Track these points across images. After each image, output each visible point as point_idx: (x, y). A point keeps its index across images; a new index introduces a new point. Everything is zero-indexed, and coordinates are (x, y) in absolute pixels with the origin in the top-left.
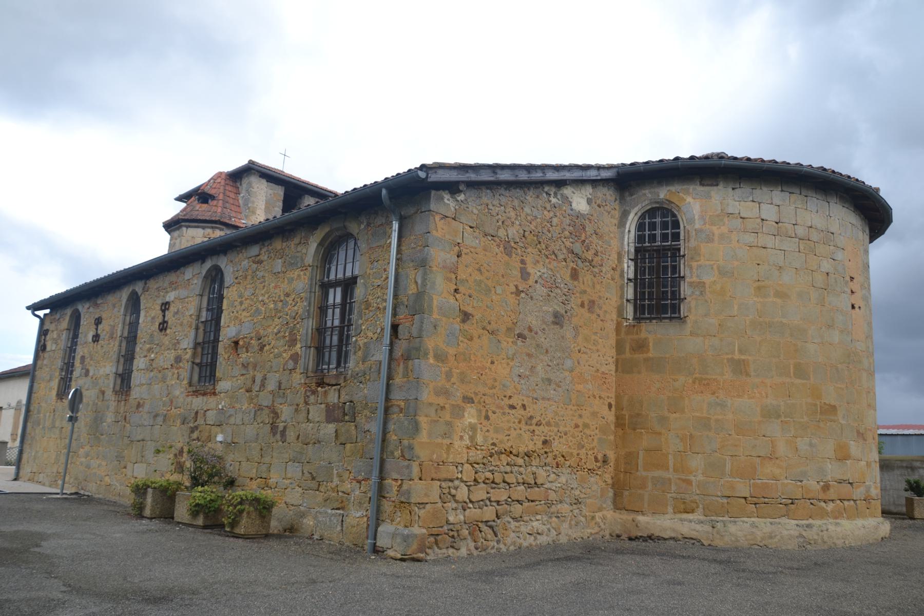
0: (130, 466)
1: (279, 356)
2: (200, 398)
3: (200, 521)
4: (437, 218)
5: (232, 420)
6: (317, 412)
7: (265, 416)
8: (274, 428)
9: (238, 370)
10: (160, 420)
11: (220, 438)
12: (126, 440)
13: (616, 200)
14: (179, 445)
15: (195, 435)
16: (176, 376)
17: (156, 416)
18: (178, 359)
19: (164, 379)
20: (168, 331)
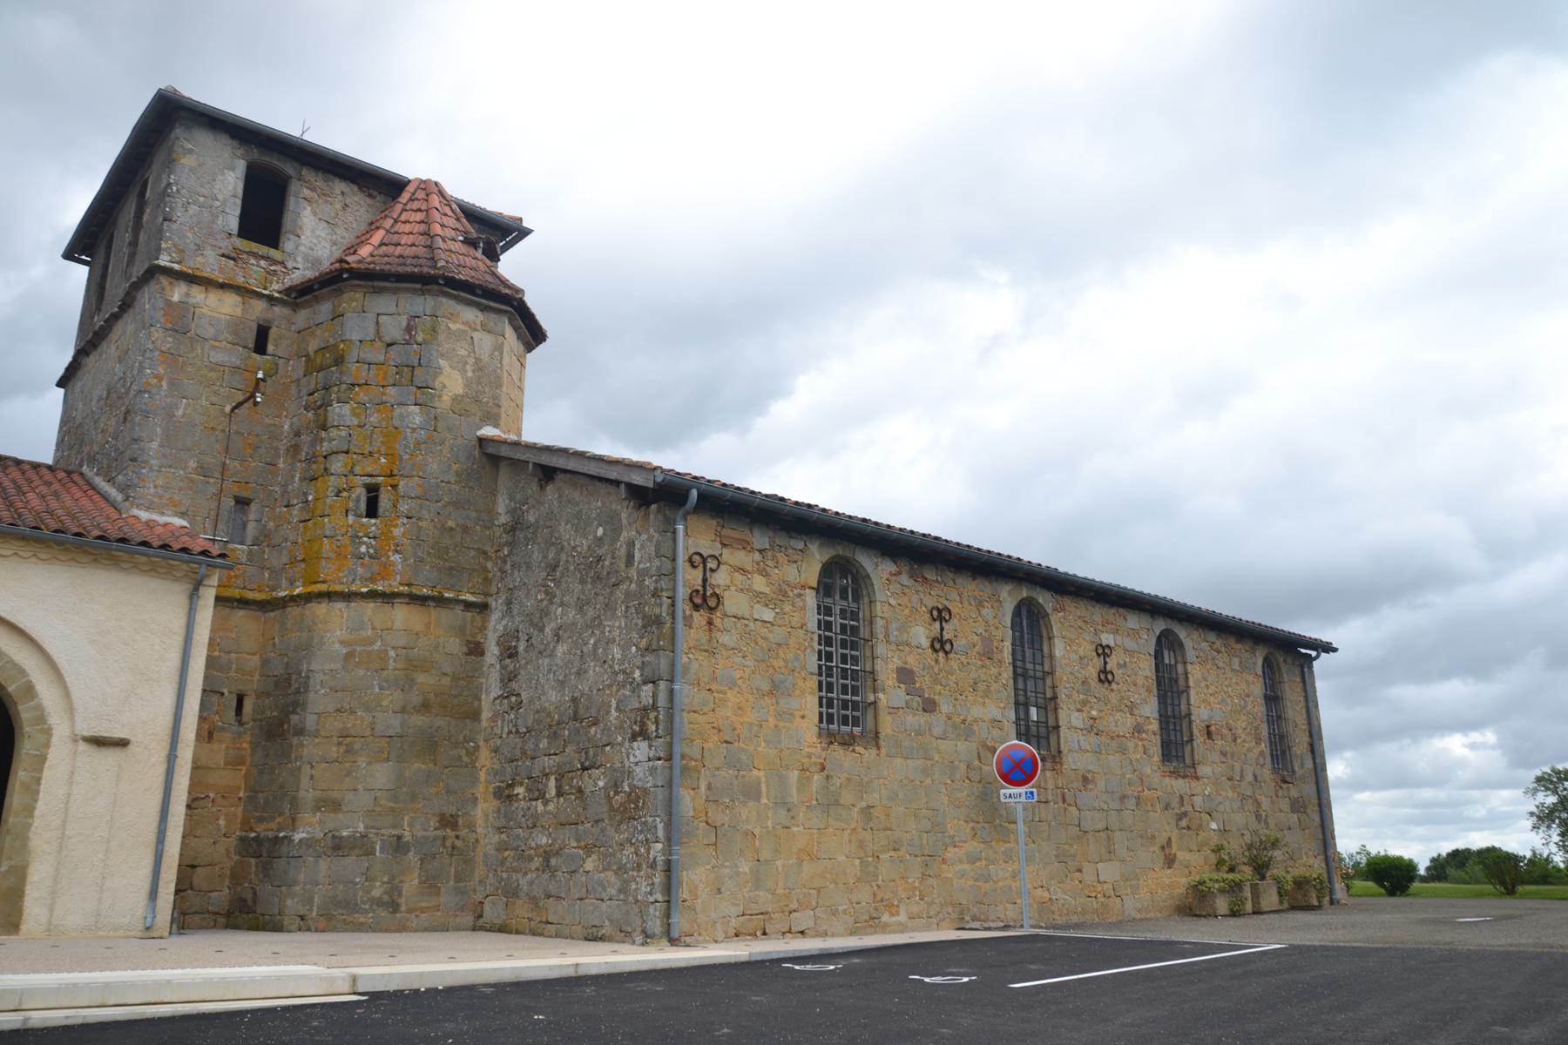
0: (1087, 867)
1: (1250, 750)
2: (1181, 781)
3: (1286, 906)
4: (584, 687)
5: (1221, 808)
6: (1285, 805)
7: (1249, 806)
8: (1258, 817)
9: (1216, 757)
10: (1131, 803)
11: (1214, 826)
12: (1074, 831)
13: (300, 732)
14: (1165, 835)
15: (1184, 823)
16: (1140, 749)
17: (1123, 798)
18: (1138, 729)
19: (1123, 751)
20: (1114, 686)
